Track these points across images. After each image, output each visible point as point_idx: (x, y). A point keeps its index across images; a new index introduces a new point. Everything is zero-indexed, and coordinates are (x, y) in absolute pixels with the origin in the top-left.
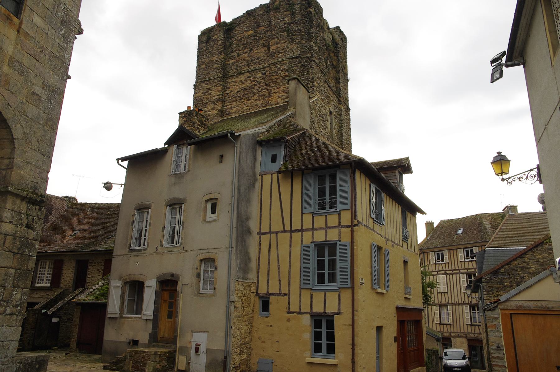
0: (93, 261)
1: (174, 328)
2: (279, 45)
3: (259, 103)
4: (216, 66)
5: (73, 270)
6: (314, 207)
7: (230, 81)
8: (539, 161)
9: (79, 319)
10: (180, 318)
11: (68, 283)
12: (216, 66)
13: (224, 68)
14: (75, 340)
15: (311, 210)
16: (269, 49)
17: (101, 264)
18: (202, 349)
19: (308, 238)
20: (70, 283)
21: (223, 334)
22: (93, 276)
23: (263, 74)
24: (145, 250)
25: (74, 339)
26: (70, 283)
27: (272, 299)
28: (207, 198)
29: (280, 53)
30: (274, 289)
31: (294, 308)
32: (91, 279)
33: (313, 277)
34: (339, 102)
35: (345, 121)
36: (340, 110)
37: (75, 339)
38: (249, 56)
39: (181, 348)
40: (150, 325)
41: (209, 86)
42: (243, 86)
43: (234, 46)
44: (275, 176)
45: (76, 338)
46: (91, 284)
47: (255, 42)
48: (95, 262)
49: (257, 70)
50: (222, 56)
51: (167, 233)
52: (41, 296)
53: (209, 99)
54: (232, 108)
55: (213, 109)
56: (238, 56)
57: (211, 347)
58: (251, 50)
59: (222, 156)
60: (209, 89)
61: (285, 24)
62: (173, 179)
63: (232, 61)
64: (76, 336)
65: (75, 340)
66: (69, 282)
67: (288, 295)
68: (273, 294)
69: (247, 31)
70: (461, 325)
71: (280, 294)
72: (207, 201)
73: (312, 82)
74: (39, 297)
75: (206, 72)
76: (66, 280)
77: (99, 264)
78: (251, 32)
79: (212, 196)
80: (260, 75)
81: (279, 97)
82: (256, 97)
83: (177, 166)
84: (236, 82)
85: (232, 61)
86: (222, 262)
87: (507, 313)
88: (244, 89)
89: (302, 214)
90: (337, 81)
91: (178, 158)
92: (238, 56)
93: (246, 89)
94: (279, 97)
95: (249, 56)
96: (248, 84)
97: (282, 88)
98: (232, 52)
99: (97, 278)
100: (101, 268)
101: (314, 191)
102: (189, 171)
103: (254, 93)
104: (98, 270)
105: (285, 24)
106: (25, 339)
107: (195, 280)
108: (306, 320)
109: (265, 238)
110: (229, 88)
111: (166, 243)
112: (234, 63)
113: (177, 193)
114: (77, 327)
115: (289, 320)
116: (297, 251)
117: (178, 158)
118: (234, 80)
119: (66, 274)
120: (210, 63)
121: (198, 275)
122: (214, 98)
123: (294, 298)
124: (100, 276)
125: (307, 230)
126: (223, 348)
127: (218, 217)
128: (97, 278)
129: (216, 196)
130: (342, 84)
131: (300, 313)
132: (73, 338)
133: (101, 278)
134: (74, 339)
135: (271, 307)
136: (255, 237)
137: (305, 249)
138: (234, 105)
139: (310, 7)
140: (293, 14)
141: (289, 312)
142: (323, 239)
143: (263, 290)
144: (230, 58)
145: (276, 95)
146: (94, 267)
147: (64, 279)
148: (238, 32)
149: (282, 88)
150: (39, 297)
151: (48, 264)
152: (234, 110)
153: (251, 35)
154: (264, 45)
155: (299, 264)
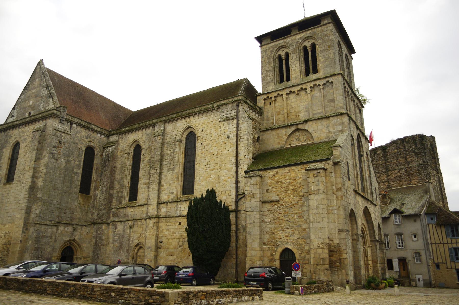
1: (408, 273)
2: (411, 158)
3: (406, 183)
4: (381, 166)
6: (451, 236)
7: (389, 172)
10: (410, 270)
12: (381, 166)
13: (386, 167)
15: (450, 237)
16: (406, 159)
18: (421, 279)
19: (450, 246)
21: (428, 275)
23: (405, 170)
24: (389, 249)
27: (440, 264)
28: (412, 233)
29: (412, 162)
30: (440, 261)
31: (449, 267)
33: (454, 258)
34: (438, 173)
35: (441, 182)
36: (439, 177)
38: (397, 162)
39: (412, 279)
40: (398, 273)
41: (380, 175)
42: (396, 175)
43: (388, 157)
44: (434, 225)
47: (398, 156)
49: (402, 169)
50: (384, 162)
51: (397, 244)
54: (393, 185)
55: (384, 185)
56: (391, 161)
57: (424, 279)
58: (397, 159)
59: (415, 220)
60: (380, 176)
61: (413, 149)
62: (396, 226)
63: (389, 164)
67: (446, 263)
68: (440, 263)
69: (394, 150)
70: (431, 233)
71: (443, 263)
72: (412, 234)
73: (430, 174)
75: (377, 168)
78: (396, 151)
79: (414, 233)
80: (404, 171)
81: (416, 182)
82: (404, 180)
83: (396, 222)
84: (392, 173)
85: (389, 164)
86: (423, 253)
87: (38, 211)
88: (397, 177)
89: (447, 238)
90: (435, 163)
91: (396, 219)
92: (391, 161)
93: (398, 177)
94: (416, 182)
95: (397, 162)
96: (399, 174)
97: (416, 178)
98: (388, 159)
101: (450, 231)
102: (402, 224)
103: (402, 179)
105: (413, 149)
107: (413, 259)
108: (454, 271)
109: (434, 246)
110: (390, 176)
111: (398, 247)
112: (390, 164)
113: (398, 231)
115: (448, 271)
116: (447, 250)
117: (396, 219)
118: (391, 172)
120: (378, 164)
121: (414, 258)
122: (384, 180)
123: (449, 264)
125: (449, 243)
126: (429, 279)
127: (418, 239)
129: (416, 233)
130: (437, 164)
131: (452, 269)
135: (440, 267)
136: (430, 245)
137: (450, 250)
138: (393, 183)
139: (423, 141)
140: (416, 145)
141: (447, 269)
142: (456, 246)
143: (436, 261)
144: (387, 162)
145: (414, 180)
148: (389, 150)
149: (416, 178)
152: (394, 185)
153: (396, 152)
154: (403, 157)
155: (448, 254)
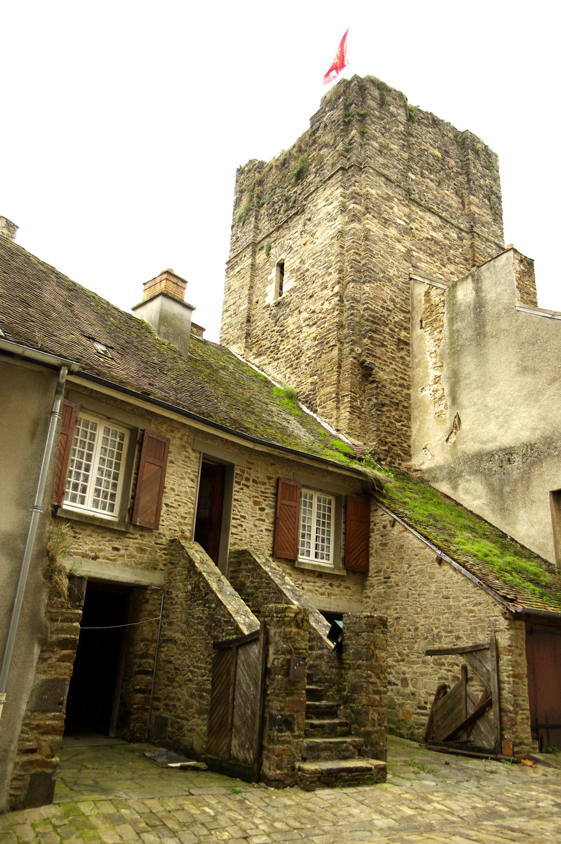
0: (243, 472)
5: (191, 484)
8: (28, 259)
9: (524, 658)
11: (180, 524)
14: (527, 719)
17: (263, 487)
20: (186, 524)
22: (244, 518)
25: (522, 714)
26: (186, 524)
32: (241, 526)
37: (526, 714)
45: (528, 713)
46: (241, 540)
48: (246, 475)
52: (92, 550)
53: (385, 305)
64: (528, 707)
65: (527, 719)
66: (182, 521)
74: (84, 556)
76: (173, 510)
77: (259, 485)
99: (255, 526)
100: (265, 500)
104: (256, 503)
106: (373, 725)
114: (526, 681)
119: (173, 489)
124: (264, 521)
128: (255, 526)
132: (521, 712)
133: (267, 530)
134: (522, 714)
146: (246, 490)
147: (167, 505)
150: (84, 556)
151: (100, 434)
